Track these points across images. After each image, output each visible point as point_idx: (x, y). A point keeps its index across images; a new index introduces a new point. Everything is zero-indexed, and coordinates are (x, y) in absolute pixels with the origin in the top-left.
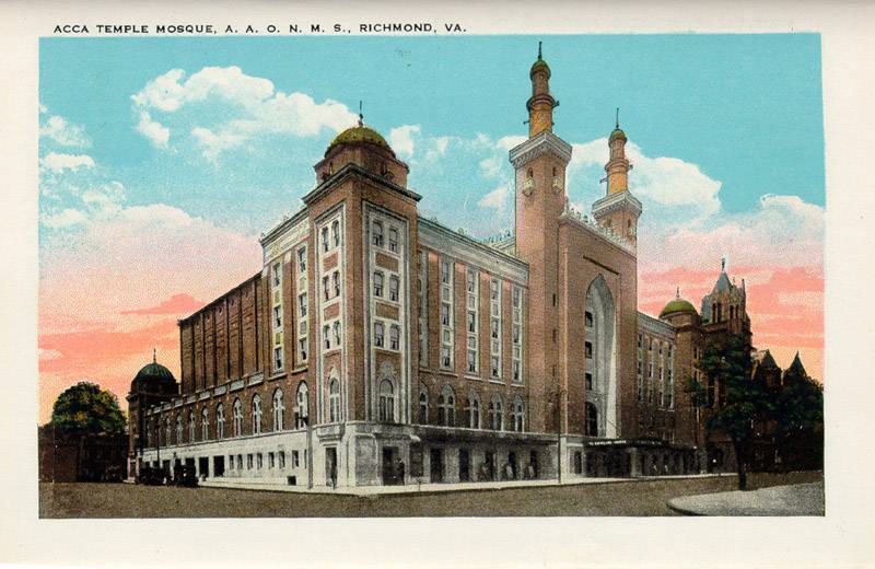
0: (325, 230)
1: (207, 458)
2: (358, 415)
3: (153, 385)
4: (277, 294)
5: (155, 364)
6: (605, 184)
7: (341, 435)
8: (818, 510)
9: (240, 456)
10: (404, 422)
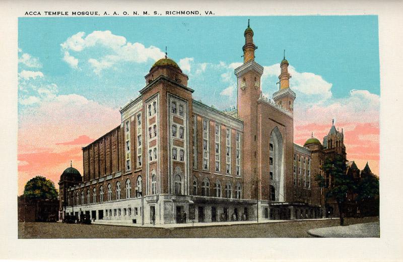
0: (150, 106)
1: (95, 211)
5: (71, 168)
10: (186, 194)
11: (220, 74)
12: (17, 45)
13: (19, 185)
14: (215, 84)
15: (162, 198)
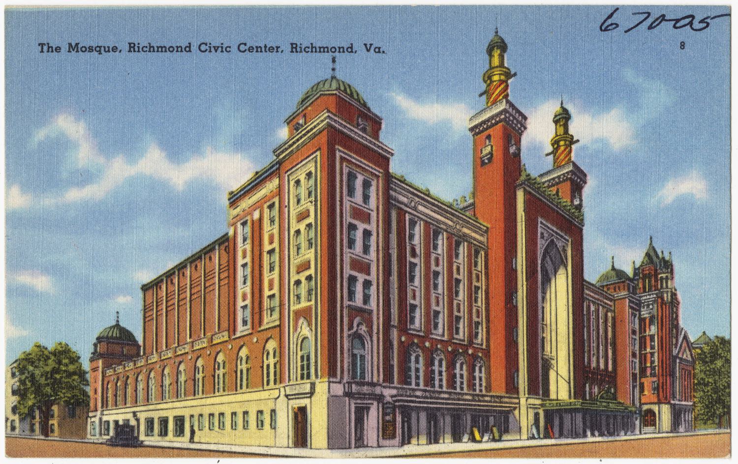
0: (298, 182)
1: (167, 417)
2: (332, 372)
3: (117, 346)
4: (244, 257)
5: (117, 325)
6: (551, 157)
7: (312, 393)
8: (726, 450)
9: (222, 414)
10: (375, 380)
11: (80, 369)
12: (383, 126)
13: (7, 361)
14: (432, 133)
15: (322, 387)
